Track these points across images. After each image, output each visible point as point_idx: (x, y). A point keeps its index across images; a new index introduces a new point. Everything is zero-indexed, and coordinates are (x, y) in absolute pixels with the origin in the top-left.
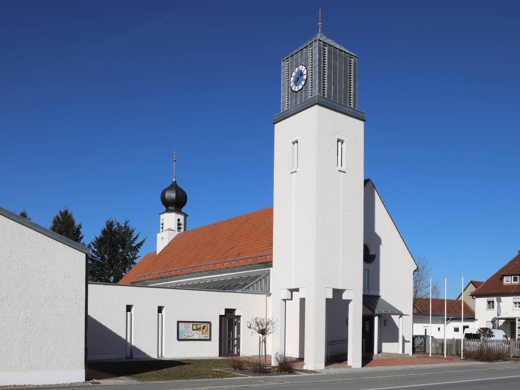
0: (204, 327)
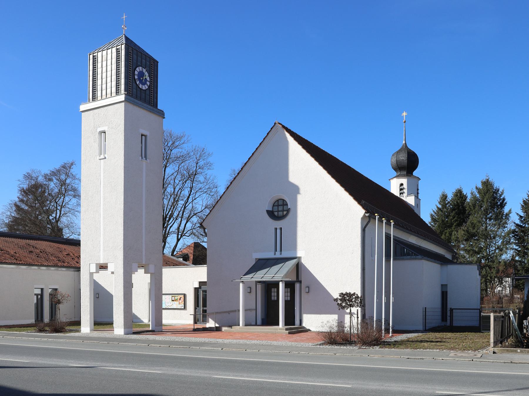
0: (181, 298)
